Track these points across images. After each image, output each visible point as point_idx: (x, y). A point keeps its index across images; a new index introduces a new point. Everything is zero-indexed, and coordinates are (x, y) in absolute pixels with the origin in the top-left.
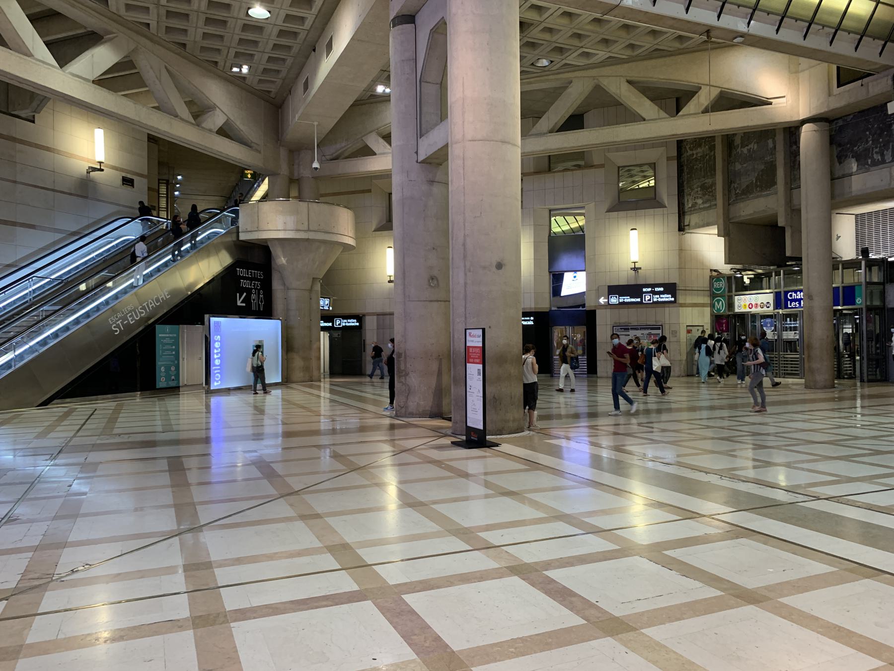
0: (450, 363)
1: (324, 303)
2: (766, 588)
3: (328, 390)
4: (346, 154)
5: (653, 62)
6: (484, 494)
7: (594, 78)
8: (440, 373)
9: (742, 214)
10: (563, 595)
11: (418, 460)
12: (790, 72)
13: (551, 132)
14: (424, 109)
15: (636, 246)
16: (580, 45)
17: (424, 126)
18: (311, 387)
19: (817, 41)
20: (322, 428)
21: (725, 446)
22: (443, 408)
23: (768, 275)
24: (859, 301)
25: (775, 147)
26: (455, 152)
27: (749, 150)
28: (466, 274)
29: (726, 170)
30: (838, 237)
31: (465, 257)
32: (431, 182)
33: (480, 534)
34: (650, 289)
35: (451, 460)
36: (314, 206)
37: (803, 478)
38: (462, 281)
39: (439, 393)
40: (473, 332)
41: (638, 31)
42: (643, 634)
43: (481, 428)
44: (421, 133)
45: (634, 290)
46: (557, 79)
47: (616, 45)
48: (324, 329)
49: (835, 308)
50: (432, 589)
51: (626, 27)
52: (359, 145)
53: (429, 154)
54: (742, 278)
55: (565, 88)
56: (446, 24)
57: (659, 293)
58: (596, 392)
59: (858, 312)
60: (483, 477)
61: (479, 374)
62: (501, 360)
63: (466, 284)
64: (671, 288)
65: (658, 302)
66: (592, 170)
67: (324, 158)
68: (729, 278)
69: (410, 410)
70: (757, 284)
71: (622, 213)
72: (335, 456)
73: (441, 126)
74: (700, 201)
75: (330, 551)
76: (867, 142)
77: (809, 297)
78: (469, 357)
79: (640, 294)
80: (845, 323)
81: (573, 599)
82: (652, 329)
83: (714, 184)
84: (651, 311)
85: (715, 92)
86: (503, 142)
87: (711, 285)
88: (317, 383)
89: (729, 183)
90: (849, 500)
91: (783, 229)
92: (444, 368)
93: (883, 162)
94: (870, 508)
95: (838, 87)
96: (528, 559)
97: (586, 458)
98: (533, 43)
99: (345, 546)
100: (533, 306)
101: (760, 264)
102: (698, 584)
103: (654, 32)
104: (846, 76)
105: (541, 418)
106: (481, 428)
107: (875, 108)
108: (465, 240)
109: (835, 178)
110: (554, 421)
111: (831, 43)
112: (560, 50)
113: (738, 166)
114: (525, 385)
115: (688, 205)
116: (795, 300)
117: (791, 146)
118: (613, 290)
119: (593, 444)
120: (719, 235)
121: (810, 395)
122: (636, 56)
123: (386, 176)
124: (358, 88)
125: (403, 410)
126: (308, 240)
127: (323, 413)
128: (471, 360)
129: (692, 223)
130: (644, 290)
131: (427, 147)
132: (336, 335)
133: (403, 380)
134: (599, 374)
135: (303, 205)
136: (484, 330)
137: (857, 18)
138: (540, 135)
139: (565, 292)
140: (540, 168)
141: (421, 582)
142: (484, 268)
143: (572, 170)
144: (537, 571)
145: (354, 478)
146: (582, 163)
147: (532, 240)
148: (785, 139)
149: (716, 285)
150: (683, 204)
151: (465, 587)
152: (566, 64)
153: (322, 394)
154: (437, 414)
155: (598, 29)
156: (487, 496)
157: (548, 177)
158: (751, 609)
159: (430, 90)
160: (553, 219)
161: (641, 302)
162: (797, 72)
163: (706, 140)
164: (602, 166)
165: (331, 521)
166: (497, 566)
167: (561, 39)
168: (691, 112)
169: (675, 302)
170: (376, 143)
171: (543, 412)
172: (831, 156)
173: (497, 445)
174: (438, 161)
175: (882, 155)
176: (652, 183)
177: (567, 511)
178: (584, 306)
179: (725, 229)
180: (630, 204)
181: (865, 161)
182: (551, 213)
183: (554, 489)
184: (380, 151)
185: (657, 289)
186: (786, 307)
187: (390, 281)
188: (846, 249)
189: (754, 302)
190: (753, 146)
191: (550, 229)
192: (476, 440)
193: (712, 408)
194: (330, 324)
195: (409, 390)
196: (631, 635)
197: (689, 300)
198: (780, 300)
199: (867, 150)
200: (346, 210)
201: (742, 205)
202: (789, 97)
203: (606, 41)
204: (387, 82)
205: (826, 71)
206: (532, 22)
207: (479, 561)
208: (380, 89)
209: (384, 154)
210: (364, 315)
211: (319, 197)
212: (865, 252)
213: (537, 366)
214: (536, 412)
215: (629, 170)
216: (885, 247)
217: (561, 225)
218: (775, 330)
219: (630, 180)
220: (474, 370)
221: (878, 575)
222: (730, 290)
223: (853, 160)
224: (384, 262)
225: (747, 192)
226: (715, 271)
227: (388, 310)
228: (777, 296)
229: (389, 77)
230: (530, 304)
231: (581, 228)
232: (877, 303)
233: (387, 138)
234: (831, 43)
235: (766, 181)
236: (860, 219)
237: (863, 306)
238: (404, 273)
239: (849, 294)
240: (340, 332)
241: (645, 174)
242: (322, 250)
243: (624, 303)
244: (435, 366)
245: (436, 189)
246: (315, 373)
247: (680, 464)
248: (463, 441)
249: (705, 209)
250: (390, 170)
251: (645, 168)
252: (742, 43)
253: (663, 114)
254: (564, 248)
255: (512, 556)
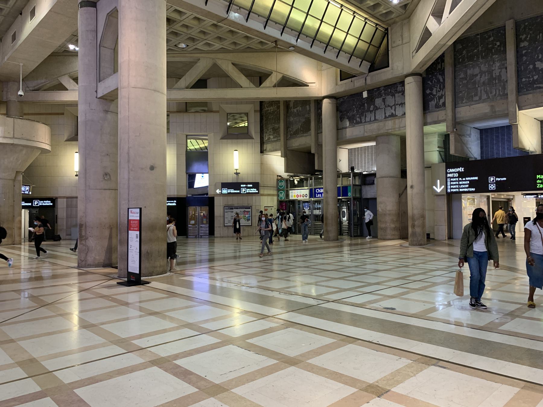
0: (117, 230)
1: (25, 189)
2: (301, 355)
3: (27, 251)
4: (45, 88)
5: (246, 54)
6: (137, 316)
7: (213, 59)
8: (110, 238)
9: (294, 145)
10: (185, 375)
11: (92, 296)
12: (318, 70)
13: (187, 88)
14: (102, 64)
15: (237, 160)
16: (205, 38)
17: (101, 75)
18: (13, 248)
19: (330, 55)
20: (22, 277)
21: (284, 274)
22: (112, 260)
23: (306, 179)
24: (349, 194)
25: (310, 110)
26: (122, 94)
27: (297, 111)
28: (129, 173)
29: (284, 120)
30: (340, 161)
31: (129, 161)
32: (106, 111)
33: (132, 341)
34: (245, 186)
35: (117, 295)
36: (19, 121)
37: (324, 290)
38: (126, 177)
39: (110, 250)
40: (134, 210)
41: (238, 35)
42: (232, 392)
43: (138, 272)
44: (100, 79)
45: (236, 185)
46: (191, 57)
47: (226, 41)
48: (24, 207)
49: (339, 198)
50: (97, 382)
51: (231, 32)
52: (55, 83)
53: (104, 94)
54: (294, 180)
55: (196, 63)
56: (118, 11)
57: (250, 188)
58: (214, 246)
59: (349, 200)
60: (138, 304)
61: (137, 237)
62: (153, 228)
63: (129, 179)
64: (256, 185)
65: (249, 193)
66: (212, 114)
67: (27, 89)
68: (287, 180)
69: (89, 263)
70: (301, 184)
71: (229, 141)
72: (32, 298)
73: (114, 76)
74: (272, 137)
75: (20, 366)
76: (354, 111)
77: (326, 192)
78: (131, 227)
79: (239, 188)
80: (343, 206)
81: (191, 376)
82: (246, 208)
83: (279, 128)
84: (245, 198)
85: (280, 76)
86: (155, 91)
87: (278, 184)
88: (19, 246)
89: (287, 127)
90: (343, 302)
91: (314, 154)
92: (114, 235)
93: (361, 122)
94: (353, 305)
95: (341, 80)
96: (163, 354)
97: (207, 288)
98: (194, 39)
99: (33, 361)
100: (176, 194)
101: (302, 173)
102: (264, 358)
103: (247, 37)
104: (344, 76)
105: (178, 264)
106: (138, 272)
107: (357, 94)
108: (129, 150)
109: (339, 129)
110: (188, 265)
111: (337, 57)
112: (193, 39)
113: (292, 119)
114: (168, 244)
115: (266, 138)
116: (320, 193)
117: (318, 110)
118: (225, 185)
119: (211, 278)
120: (282, 156)
121: (326, 244)
122: (238, 49)
123: (74, 105)
124: (56, 44)
125: (84, 263)
126: (12, 144)
127: (23, 267)
128: (132, 229)
129: (268, 149)
130: (242, 186)
131: (104, 88)
132: (34, 211)
133: (83, 242)
134: (215, 236)
135: (10, 120)
136: (141, 209)
137: (349, 46)
138: (180, 89)
139: (196, 186)
140: (179, 110)
141: (88, 379)
142: (142, 169)
143: (200, 112)
144: (169, 361)
145: (44, 312)
146: (206, 109)
147: (176, 153)
148: (315, 106)
149: (280, 184)
150: (263, 138)
151: (120, 378)
152: (196, 49)
153: (23, 253)
154: (109, 264)
155: (215, 30)
156: (141, 316)
157: (185, 114)
158: (292, 369)
159: (106, 53)
160: (189, 141)
161: (240, 193)
162: (321, 70)
163: (275, 103)
164: (217, 112)
165: (22, 343)
166: (143, 361)
167: (194, 33)
168: (268, 86)
169: (258, 193)
170: (67, 82)
171: (179, 261)
172: (337, 117)
173: (148, 283)
174: (111, 99)
175: (361, 119)
176: (246, 124)
177: (191, 321)
178: (207, 194)
179: (285, 153)
180: (234, 135)
181: (354, 122)
182: (187, 137)
183: (187, 307)
184: (71, 88)
185: (249, 186)
186: (315, 197)
187: (76, 175)
188: (344, 167)
189: (299, 194)
190: (299, 108)
191: (187, 147)
192: (134, 280)
193: (249, 256)
194: (30, 204)
195: (88, 249)
196: (225, 394)
197: (266, 192)
198: (312, 193)
199: (354, 115)
200: (43, 125)
201: (293, 140)
202: (317, 83)
203: (220, 38)
204: (76, 43)
205: (334, 72)
206: (175, 20)
207: (134, 359)
208: (72, 47)
209: (74, 90)
210: (57, 198)
211: (22, 115)
212: (352, 169)
213: (176, 232)
214: (175, 260)
215: (233, 116)
216: (362, 167)
217: (194, 145)
218: (310, 209)
219: (234, 121)
220: (134, 235)
221: (355, 341)
222: (287, 187)
223: (347, 120)
224: (72, 163)
225: (296, 134)
226: (280, 176)
227: (74, 195)
228: (311, 190)
229: (77, 40)
230: (174, 193)
231: (206, 148)
232: (358, 195)
233: (76, 80)
234: (337, 57)
235: (306, 128)
236: (350, 151)
237: (352, 197)
238: (86, 170)
239: (344, 191)
240: (37, 210)
241: (243, 119)
242: (24, 152)
243: (230, 193)
244: (107, 233)
245: (109, 116)
246: (17, 239)
247: (259, 287)
248: (125, 282)
249: (274, 141)
250: (77, 102)
251: (243, 115)
252: (294, 50)
253: (252, 85)
254: (194, 160)
255: (154, 353)
